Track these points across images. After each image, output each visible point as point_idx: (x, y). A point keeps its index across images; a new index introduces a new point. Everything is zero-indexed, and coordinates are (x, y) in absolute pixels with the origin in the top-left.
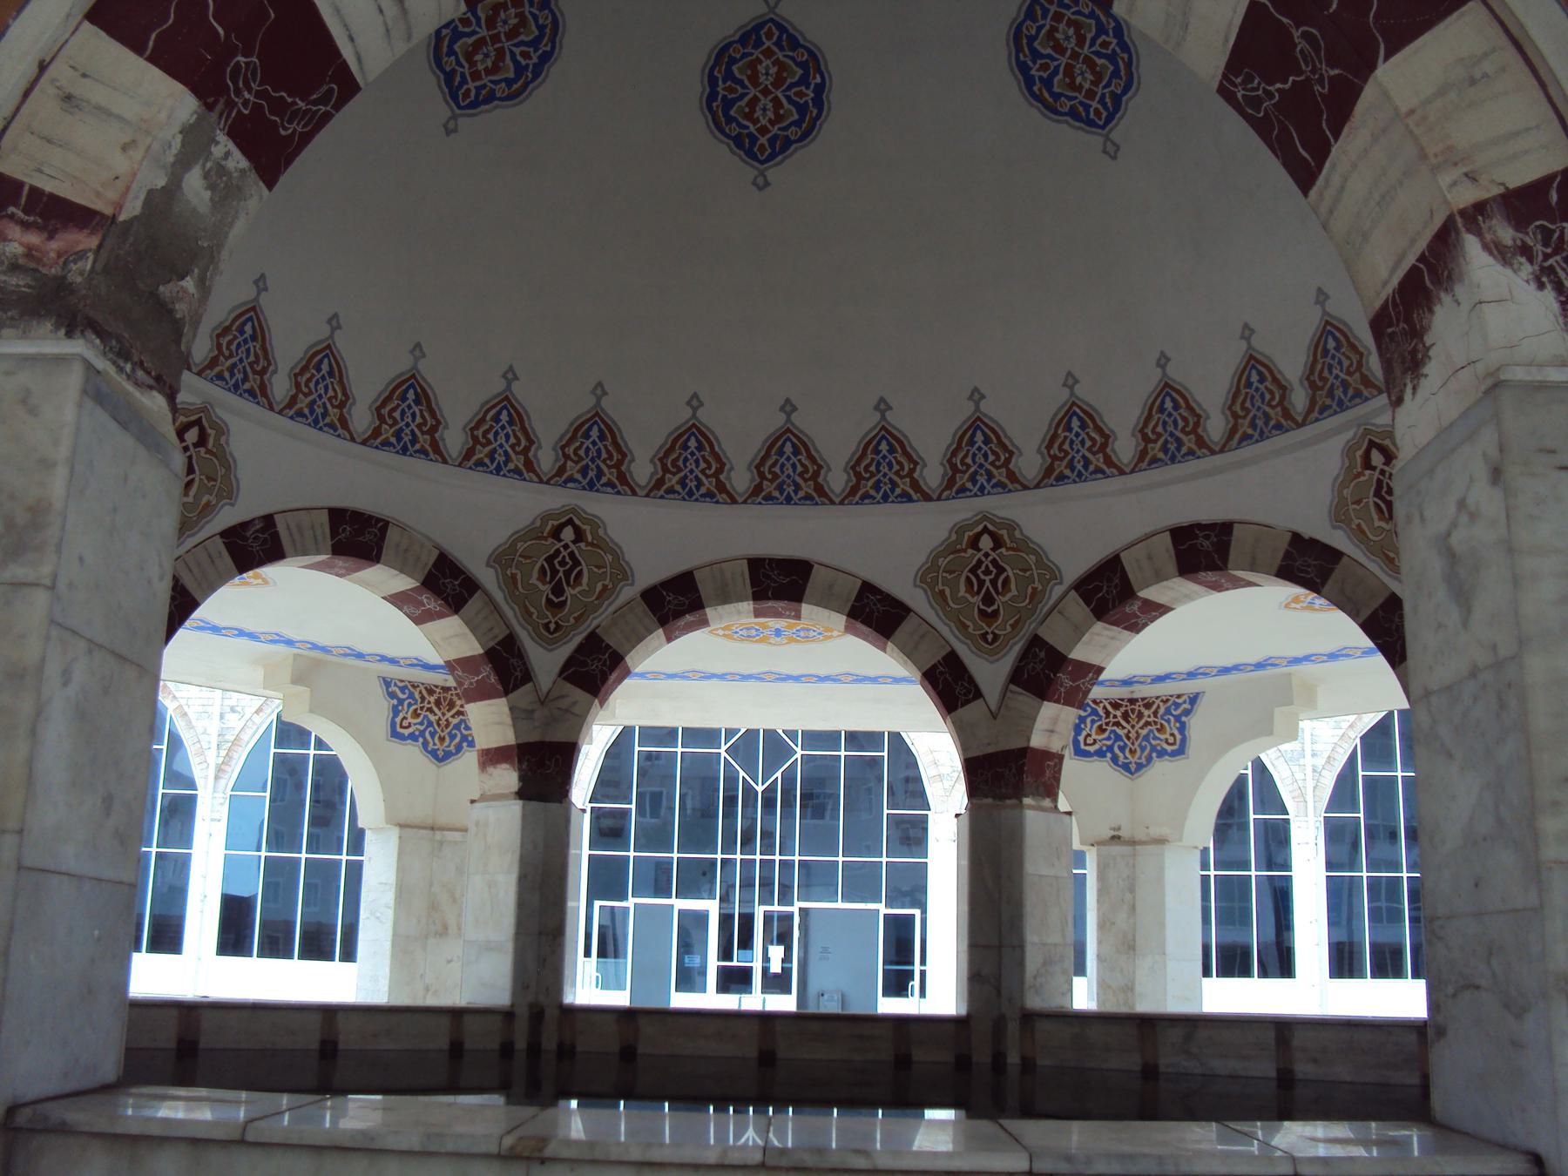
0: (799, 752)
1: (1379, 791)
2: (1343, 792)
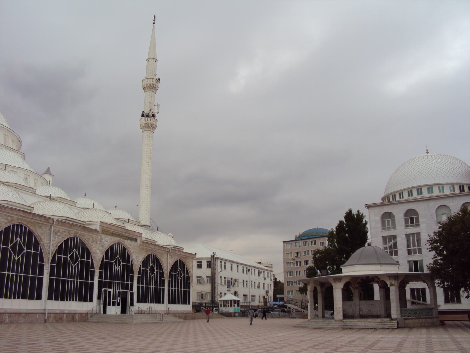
0: (25, 250)
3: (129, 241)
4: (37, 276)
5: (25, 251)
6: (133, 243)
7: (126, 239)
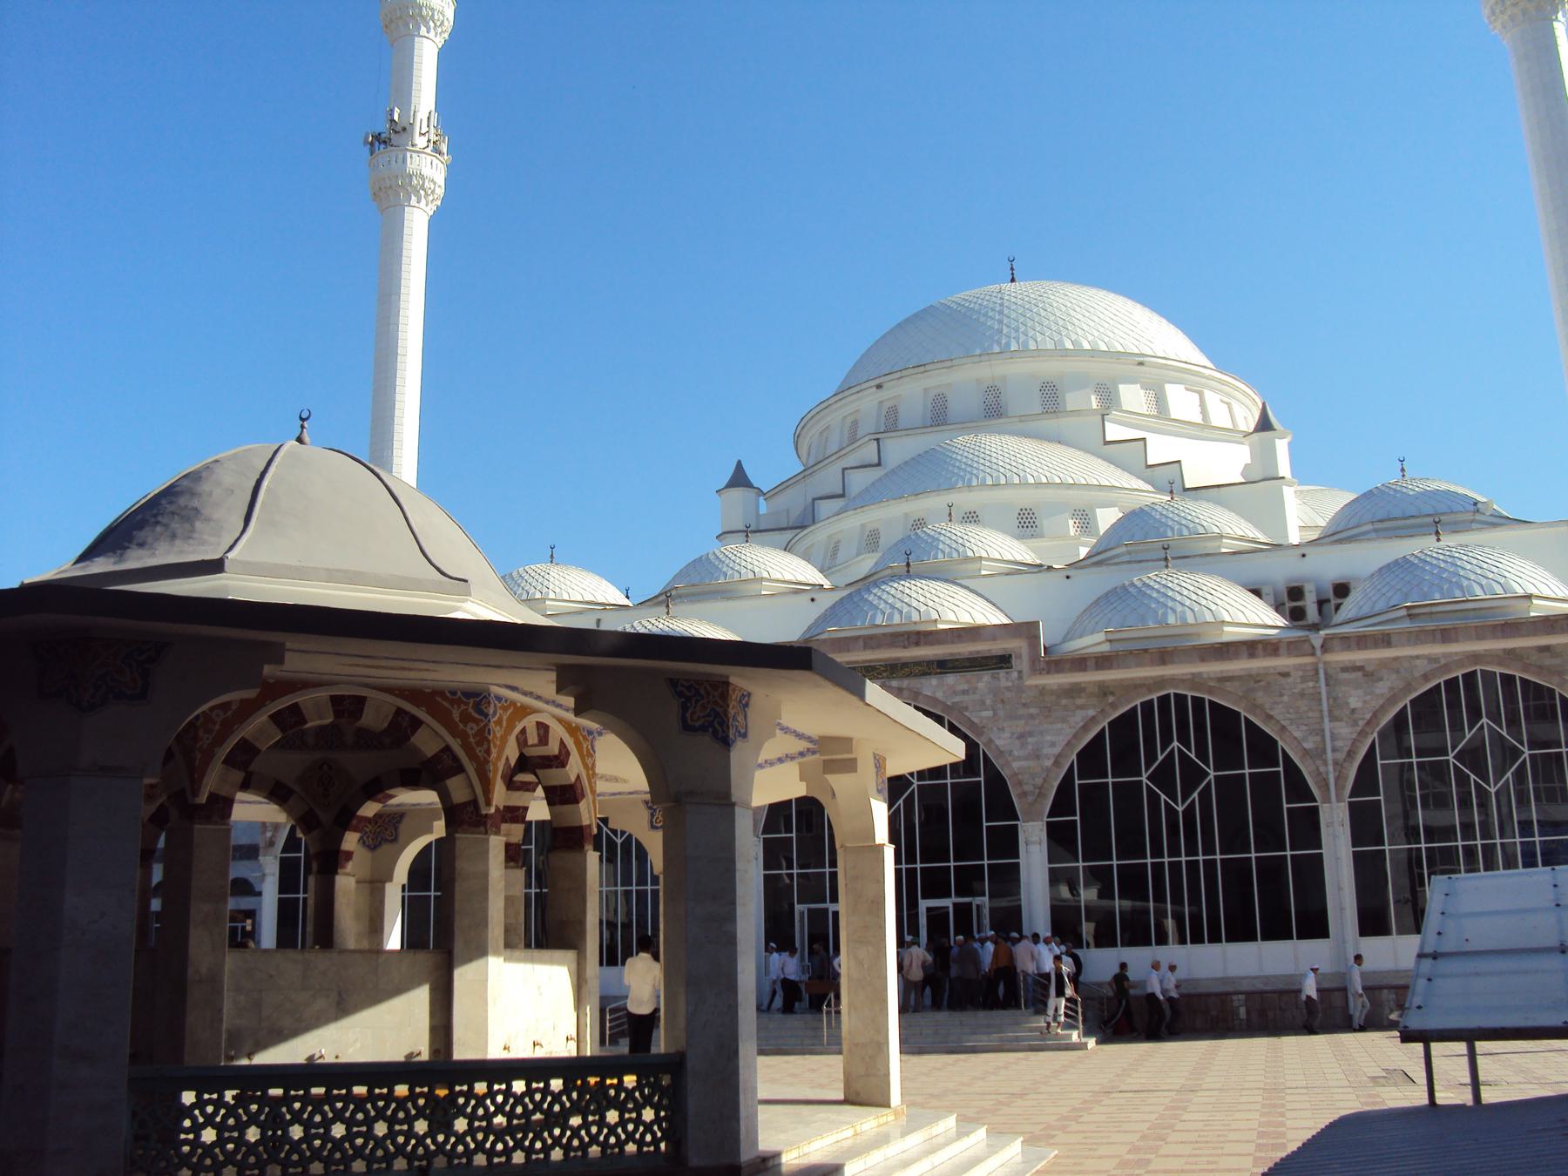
1: (1093, 796)
2: (1062, 802)
3: (950, 679)
4: (1115, 863)
5: (1211, 777)
6: (984, 680)
7: (924, 674)
